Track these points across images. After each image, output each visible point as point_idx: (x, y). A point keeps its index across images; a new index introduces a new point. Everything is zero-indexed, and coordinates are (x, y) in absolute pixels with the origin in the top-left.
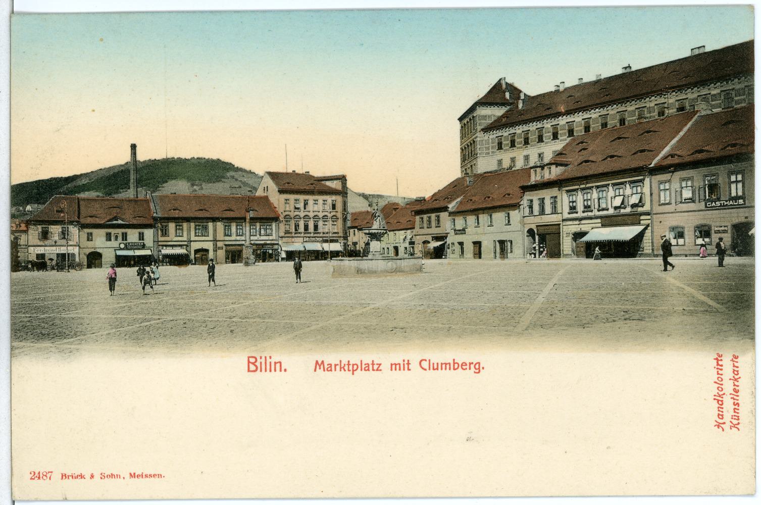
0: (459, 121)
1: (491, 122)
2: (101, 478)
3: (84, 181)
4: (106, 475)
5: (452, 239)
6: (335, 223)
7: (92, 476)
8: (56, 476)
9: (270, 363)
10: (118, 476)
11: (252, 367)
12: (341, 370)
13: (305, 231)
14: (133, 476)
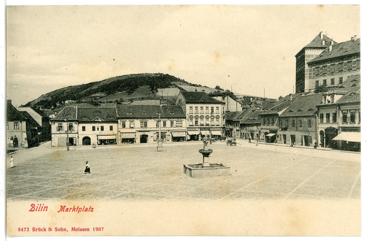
0: (295, 57)
1: (313, 59)
5: (280, 133)
6: (218, 120)
9: (42, 207)
10: (65, 230)
11: (19, 230)
12: (72, 211)
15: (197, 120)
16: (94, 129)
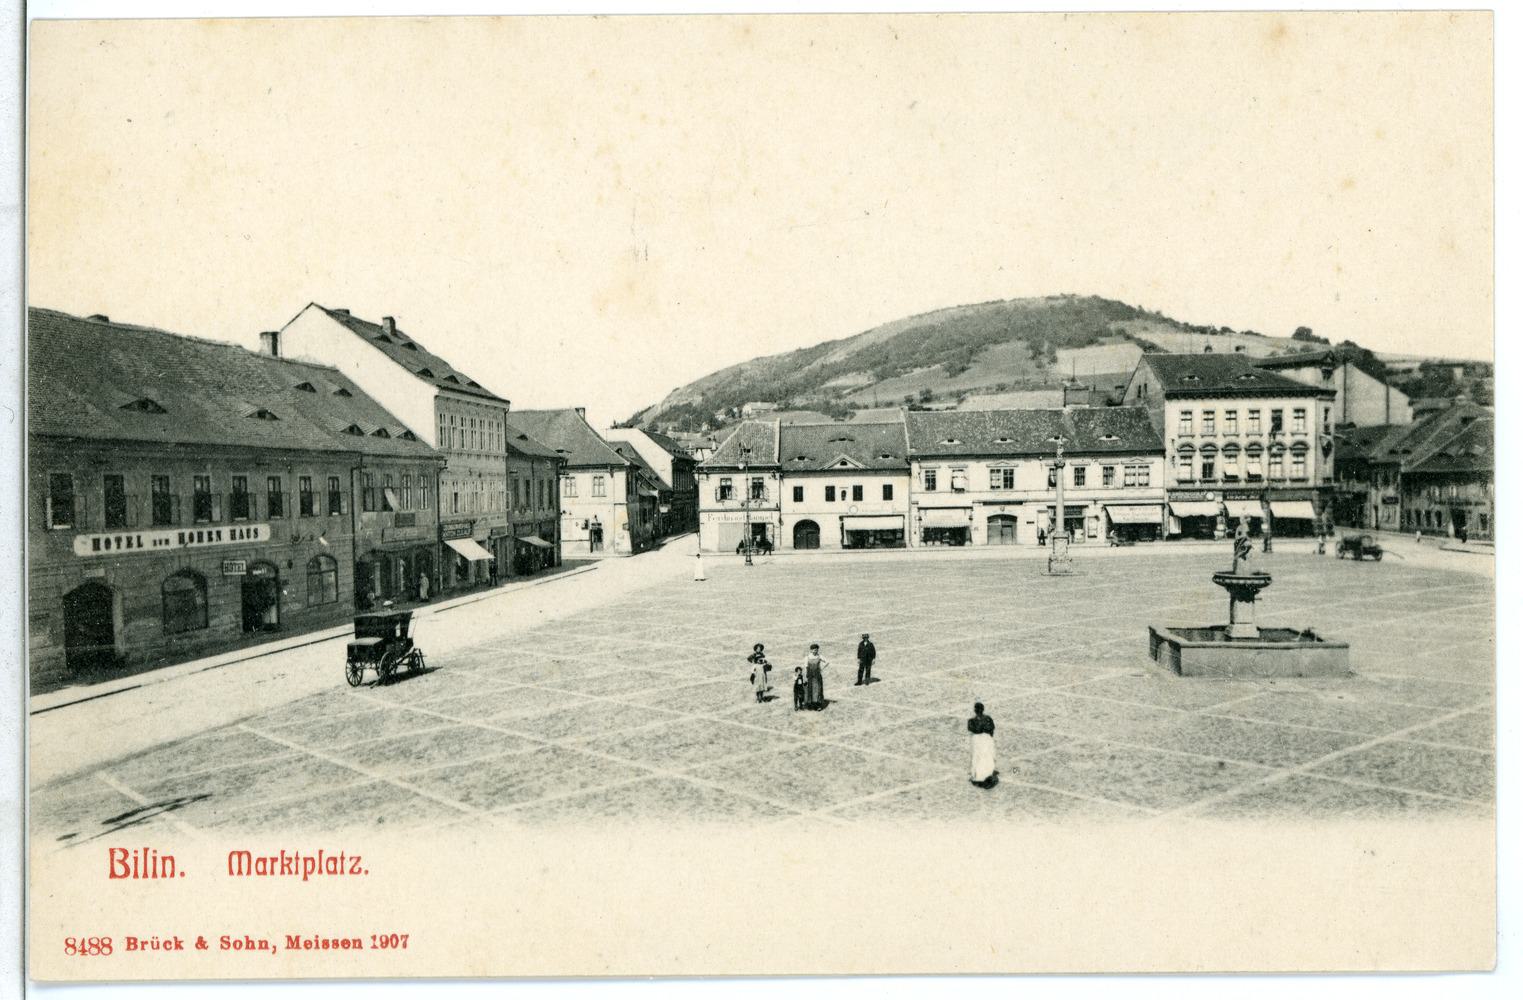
2: (222, 947)
3: (838, 357)
4: (232, 941)
7: (201, 944)
8: (119, 945)
9: (155, 859)
13: (1204, 476)
14: (293, 943)
15: (1210, 461)
16: (830, 494)
